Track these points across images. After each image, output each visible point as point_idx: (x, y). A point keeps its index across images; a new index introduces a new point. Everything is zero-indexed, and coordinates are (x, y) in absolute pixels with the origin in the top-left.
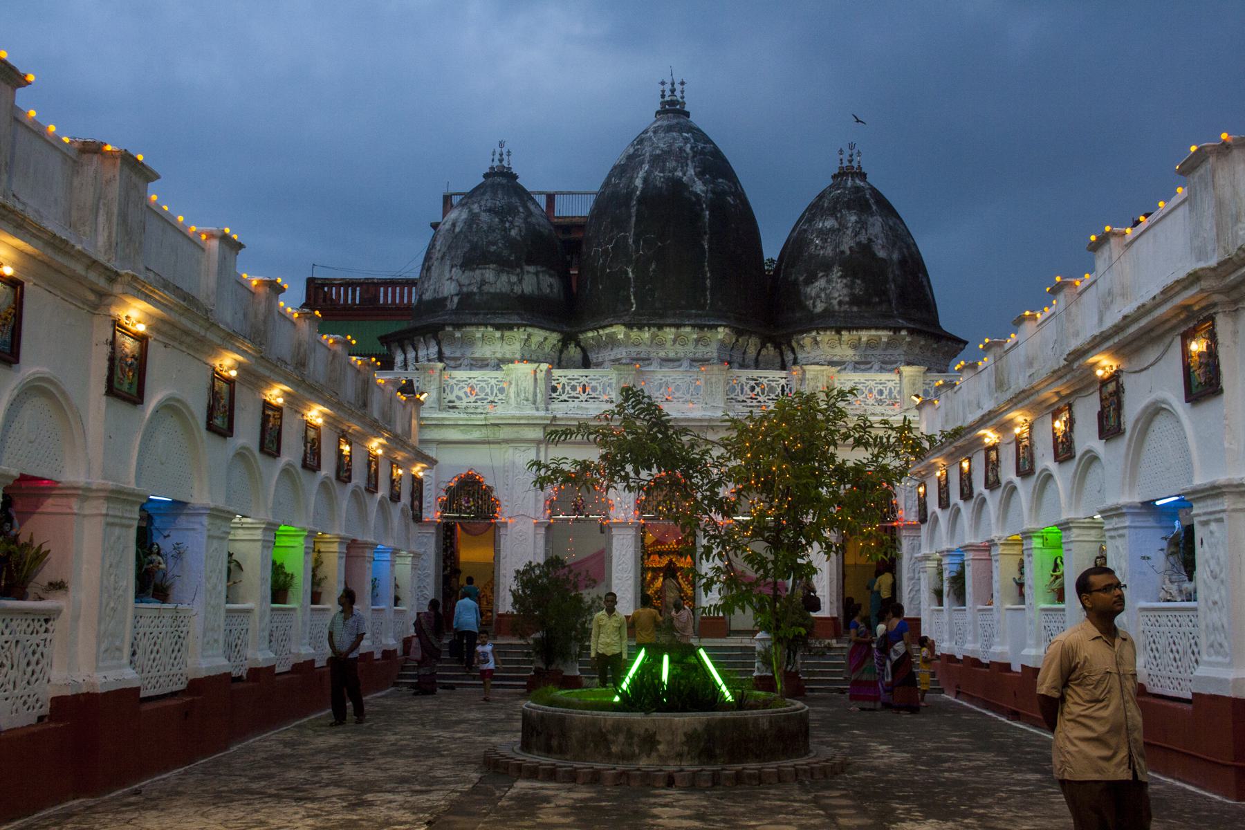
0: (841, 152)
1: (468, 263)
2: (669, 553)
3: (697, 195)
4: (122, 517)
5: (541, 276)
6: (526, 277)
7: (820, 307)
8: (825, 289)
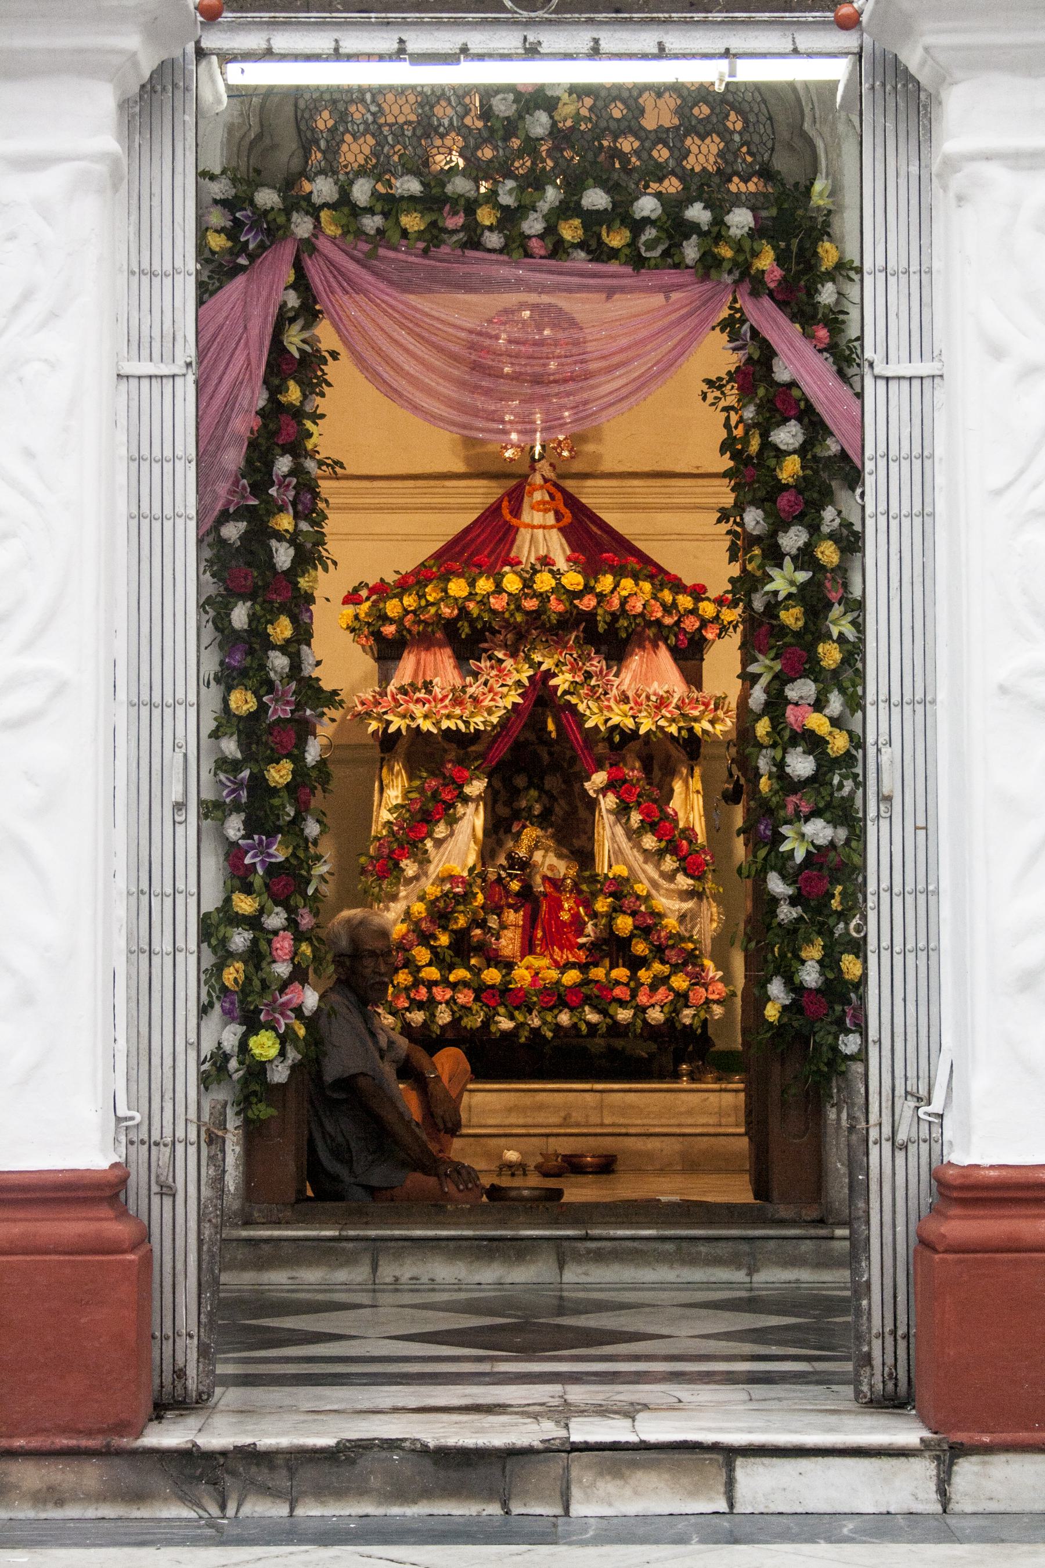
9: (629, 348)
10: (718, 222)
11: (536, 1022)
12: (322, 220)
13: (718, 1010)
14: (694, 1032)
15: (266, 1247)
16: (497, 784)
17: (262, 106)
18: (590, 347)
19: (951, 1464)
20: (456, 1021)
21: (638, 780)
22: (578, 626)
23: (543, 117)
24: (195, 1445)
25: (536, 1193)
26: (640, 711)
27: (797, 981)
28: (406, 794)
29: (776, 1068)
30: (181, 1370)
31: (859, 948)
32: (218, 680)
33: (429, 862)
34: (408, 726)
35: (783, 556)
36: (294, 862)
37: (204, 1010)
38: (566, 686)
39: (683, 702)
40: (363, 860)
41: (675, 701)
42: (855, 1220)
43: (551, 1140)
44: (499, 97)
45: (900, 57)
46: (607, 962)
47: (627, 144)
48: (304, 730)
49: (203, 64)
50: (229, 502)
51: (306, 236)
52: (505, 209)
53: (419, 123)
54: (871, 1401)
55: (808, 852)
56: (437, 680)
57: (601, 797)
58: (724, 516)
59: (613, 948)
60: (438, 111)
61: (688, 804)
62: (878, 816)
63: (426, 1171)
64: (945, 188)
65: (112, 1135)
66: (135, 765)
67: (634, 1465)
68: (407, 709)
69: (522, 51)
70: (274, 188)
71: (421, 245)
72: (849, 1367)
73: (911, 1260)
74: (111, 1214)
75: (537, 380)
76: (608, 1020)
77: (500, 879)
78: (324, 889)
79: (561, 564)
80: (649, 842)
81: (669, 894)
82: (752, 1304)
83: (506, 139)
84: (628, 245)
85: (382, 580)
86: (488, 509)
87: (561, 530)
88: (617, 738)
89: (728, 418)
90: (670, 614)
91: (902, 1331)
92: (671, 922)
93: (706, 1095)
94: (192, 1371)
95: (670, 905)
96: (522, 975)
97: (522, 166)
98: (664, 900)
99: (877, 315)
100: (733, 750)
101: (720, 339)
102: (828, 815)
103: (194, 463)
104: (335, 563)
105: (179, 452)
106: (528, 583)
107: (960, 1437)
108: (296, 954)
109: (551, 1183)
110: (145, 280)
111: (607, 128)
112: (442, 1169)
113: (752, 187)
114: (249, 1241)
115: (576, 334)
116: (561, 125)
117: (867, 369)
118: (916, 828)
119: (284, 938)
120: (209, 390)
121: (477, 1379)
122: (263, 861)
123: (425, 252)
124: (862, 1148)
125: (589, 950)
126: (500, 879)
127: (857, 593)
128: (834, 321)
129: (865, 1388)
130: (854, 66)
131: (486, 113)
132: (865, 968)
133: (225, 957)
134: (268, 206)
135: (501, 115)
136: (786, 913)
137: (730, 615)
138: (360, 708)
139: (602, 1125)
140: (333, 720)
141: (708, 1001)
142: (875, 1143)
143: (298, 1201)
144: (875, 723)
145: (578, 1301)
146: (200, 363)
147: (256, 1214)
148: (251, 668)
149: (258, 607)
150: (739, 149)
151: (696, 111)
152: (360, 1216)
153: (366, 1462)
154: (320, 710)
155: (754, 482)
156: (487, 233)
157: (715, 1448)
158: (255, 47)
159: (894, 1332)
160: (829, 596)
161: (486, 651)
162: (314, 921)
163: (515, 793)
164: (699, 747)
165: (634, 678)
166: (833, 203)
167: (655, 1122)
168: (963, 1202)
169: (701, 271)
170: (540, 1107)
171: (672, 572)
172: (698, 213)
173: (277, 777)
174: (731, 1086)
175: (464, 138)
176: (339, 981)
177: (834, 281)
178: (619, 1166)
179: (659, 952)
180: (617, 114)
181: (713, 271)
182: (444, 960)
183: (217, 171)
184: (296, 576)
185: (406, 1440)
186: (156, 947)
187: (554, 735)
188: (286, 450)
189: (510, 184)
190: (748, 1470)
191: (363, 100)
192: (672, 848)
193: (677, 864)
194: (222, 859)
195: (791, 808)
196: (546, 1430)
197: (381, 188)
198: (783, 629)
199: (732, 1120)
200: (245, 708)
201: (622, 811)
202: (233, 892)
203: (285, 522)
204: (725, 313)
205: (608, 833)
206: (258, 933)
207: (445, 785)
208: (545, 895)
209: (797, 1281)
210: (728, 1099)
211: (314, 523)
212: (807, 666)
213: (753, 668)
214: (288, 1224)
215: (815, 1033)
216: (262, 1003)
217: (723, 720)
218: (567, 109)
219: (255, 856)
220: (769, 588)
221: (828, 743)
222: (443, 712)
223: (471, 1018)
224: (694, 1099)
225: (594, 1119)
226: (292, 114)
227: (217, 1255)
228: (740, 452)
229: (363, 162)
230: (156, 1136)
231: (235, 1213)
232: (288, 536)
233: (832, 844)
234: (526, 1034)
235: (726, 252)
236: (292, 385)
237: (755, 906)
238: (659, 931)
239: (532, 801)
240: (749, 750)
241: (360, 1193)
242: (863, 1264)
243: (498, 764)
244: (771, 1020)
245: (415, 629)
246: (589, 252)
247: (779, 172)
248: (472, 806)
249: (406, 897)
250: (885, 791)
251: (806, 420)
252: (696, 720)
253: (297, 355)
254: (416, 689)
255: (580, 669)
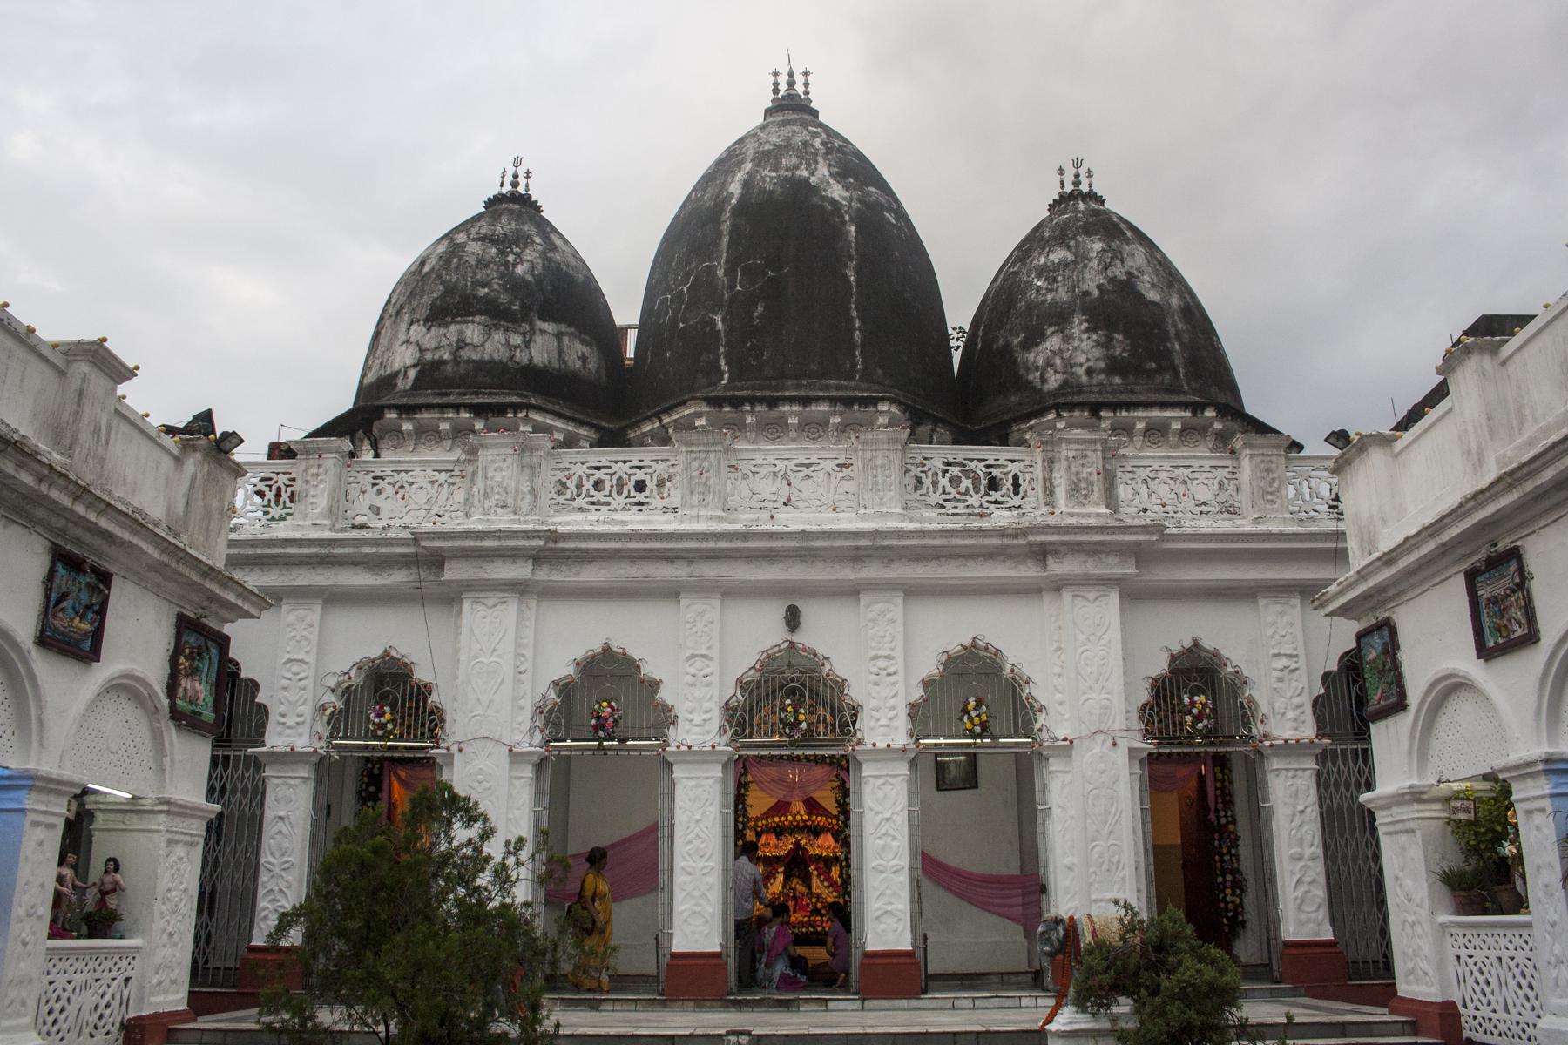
0: (1061, 171)
1: (438, 315)
2: (794, 829)
3: (833, 202)
4: (45, 813)
5: (566, 340)
6: (538, 338)
7: (1054, 381)
8: (1060, 351)
239: (796, 872)
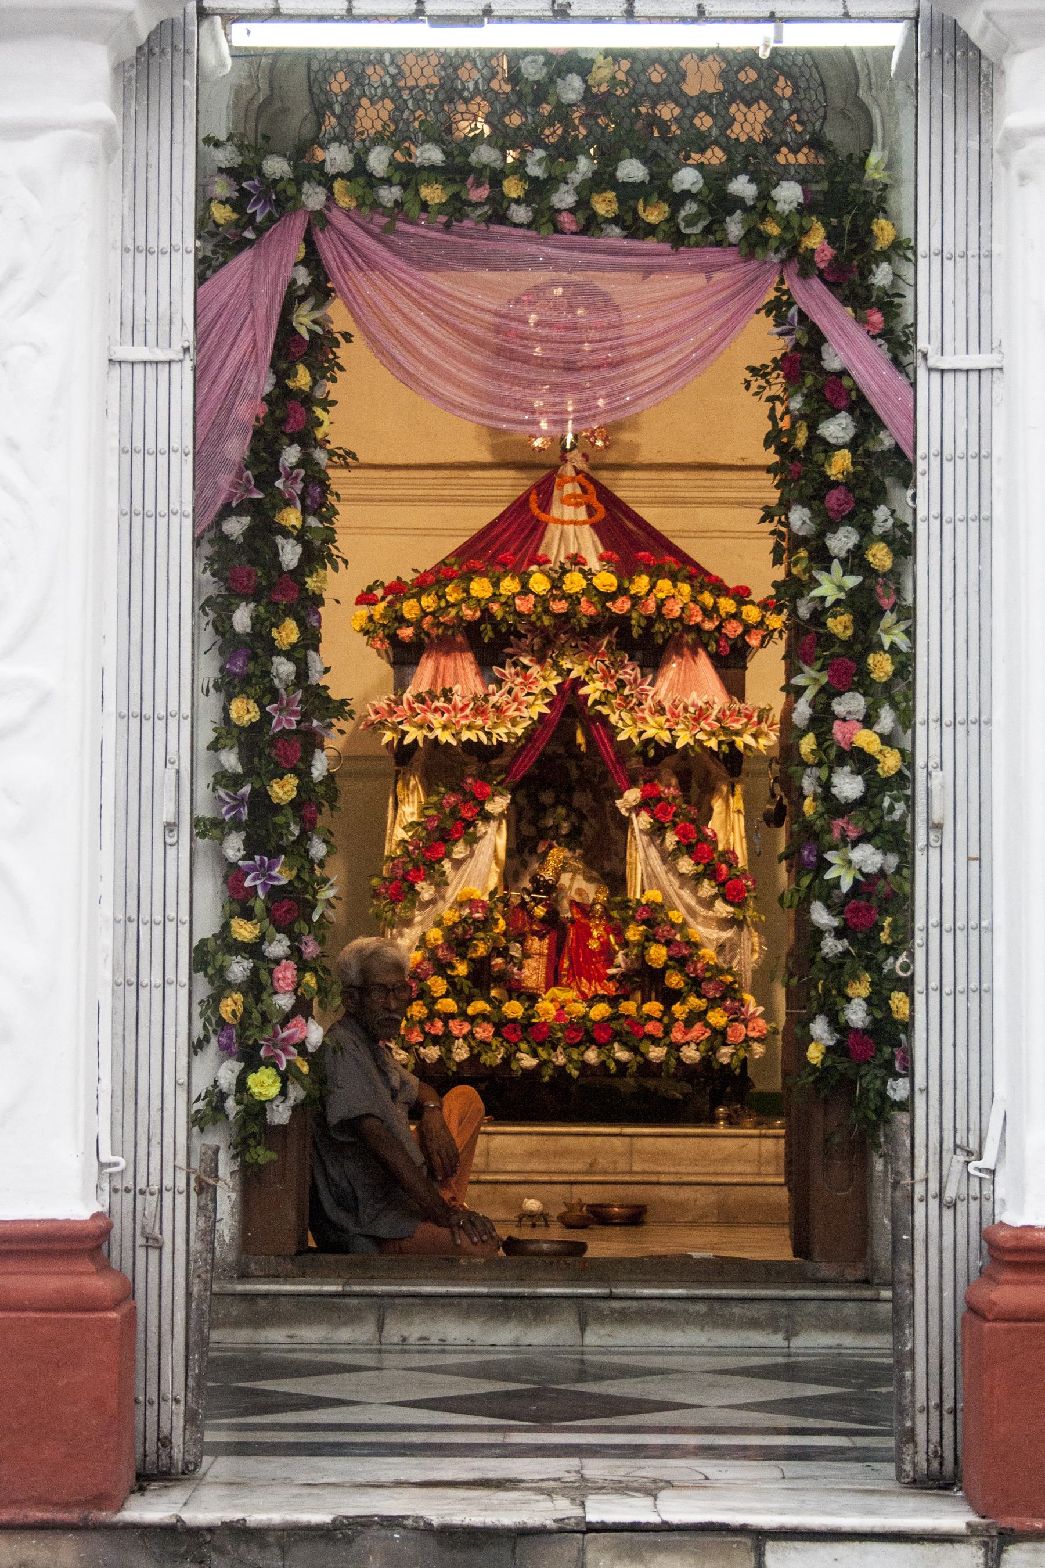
9: (667, 332)
10: (764, 196)
11: (561, 1060)
12: (336, 191)
13: (758, 1049)
14: (732, 1071)
15: (263, 1303)
16: (522, 800)
17: (274, 64)
18: (627, 330)
19: (1001, 1551)
20: (474, 1058)
21: (674, 798)
22: (610, 631)
23: (575, 81)
24: (179, 1520)
25: (556, 1246)
26: (677, 724)
27: (842, 1020)
28: (422, 811)
29: (819, 1116)
30: (166, 1438)
31: (907, 985)
32: (218, 687)
33: (447, 884)
34: (426, 737)
35: (831, 558)
36: (297, 884)
37: (196, 1047)
38: (597, 695)
39: (724, 713)
40: (375, 882)
41: (715, 713)
42: (900, 1282)
43: (575, 1188)
44: (529, 59)
45: (961, 23)
46: (638, 995)
47: (667, 111)
48: (311, 742)
49: (206, 24)
50: (232, 495)
51: (318, 207)
52: (534, 180)
53: (442, 86)
54: (914, 1481)
55: (856, 881)
56: (457, 688)
57: (633, 816)
58: (768, 515)
59: (645, 980)
60: (463, 73)
61: (728, 824)
62: (928, 845)
63: (437, 1221)
64: (1007, 165)
65: (94, 1182)
66: (123, 781)
67: (656, 1548)
68: (424, 719)
69: (550, 14)
70: (285, 156)
71: (442, 219)
72: (890, 1442)
73: (959, 1328)
74: (92, 1268)
75: (571, 367)
76: (640, 1059)
77: (523, 904)
78: (330, 913)
79: (593, 563)
80: (686, 865)
81: (707, 922)
82: (789, 1372)
83: (537, 103)
84: (667, 220)
85: (399, 578)
86: (515, 502)
87: (595, 526)
88: (652, 753)
89: (773, 409)
90: (711, 619)
91: (948, 1404)
92: (709, 953)
93: (744, 1141)
94: (178, 1439)
95: (707, 934)
96: (546, 1008)
97: (553, 133)
98: (700, 928)
99: (933, 300)
100: (776, 767)
101: (766, 323)
102: (877, 840)
103: (191, 456)
104: (346, 562)
105: (175, 445)
106: (556, 584)
107: (1011, 1522)
108: (299, 985)
109: (575, 1236)
110: (140, 258)
111: (646, 94)
112: (454, 1219)
113: (801, 159)
114: (245, 1296)
115: (612, 317)
116: (595, 90)
117: (920, 361)
118: (969, 859)
119: (286, 968)
120: (211, 374)
121: (485, 1451)
122: (264, 884)
123: (447, 227)
124: (907, 1206)
125: (620, 982)
126: (523, 904)
127: (910, 602)
128: (889, 304)
129: (908, 1467)
130: (910, 30)
131: (515, 77)
132: (912, 1010)
133: (222, 986)
134: (277, 176)
135: (531, 78)
136: (831, 946)
137: (775, 621)
138: (373, 717)
139: (631, 1172)
140: (342, 732)
141: (748, 1039)
142: (921, 1200)
143: (299, 1253)
144: (926, 743)
145: (602, 1366)
146: (198, 349)
147: (252, 1266)
148: (253, 674)
149: (261, 609)
150: (788, 117)
151: (742, 76)
152: (364, 1270)
153: (366, 1540)
154: (328, 720)
155: (800, 478)
156: (514, 206)
157: (743, 1530)
158: (262, 7)
159: (940, 1406)
160: (881, 602)
161: (511, 656)
162: (319, 950)
163: (541, 810)
164: (741, 763)
165: (670, 688)
166: (890, 177)
167: (689, 1169)
168: (1016, 1266)
169: (745, 250)
170: (565, 1152)
171: (714, 573)
172: (742, 187)
173: (281, 793)
174: (771, 1132)
175: (490, 104)
176: (348, 1014)
177: (889, 260)
178: (648, 1218)
179: (696, 985)
180: (656, 78)
181: (759, 251)
182: (461, 991)
183: (223, 137)
184: (303, 575)
185: (408, 1517)
186: (144, 979)
187: (583, 748)
188: (293, 440)
189: (540, 153)
190: (780, 1556)
191: (381, 62)
192: (710, 872)
193: (716, 890)
194: (220, 881)
195: (837, 833)
196: (562, 1509)
197: (399, 157)
198: (831, 637)
199: (772, 1169)
200: (247, 718)
201: (657, 831)
202: (231, 917)
203: (292, 517)
204: (772, 295)
205: (641, 854)
206: (259, 963)
207: (465, 802)
208: (573, 921)
209: (839, 1347)
210: (769, 1145)
211: (323, 519)
212: (856, 679)
213: (798, 680)
214: (287, 1277)
215: (861, 1077)
216: (263, 1038)
217: (767, 735)
218: (602, 73)
219: (255, 879)
220: (816, 593)
221: (878, 762)
222: (463, 722)
223: (490, 1054)
224: (730, 1146)
225: (623, 1166)
226: (304, 76)
227: (207, 1311)
228: (787, 445)
229: (380, 129)
230: (141, 1184)
231: (230, 1265)
232: (295, 532)
233: (882, 873)
234: (550, 1072)
235: (773, 229)
236: (301, 369)
237: (797, 939)
238: (695, 962)
239: (559, 818)
240: (793, 769)
241: (362, 1243)
242: (907, 1332)
243: (523, 777)
244: (814, 1062)
245: (434, 632)
246: (623, 228)
247: (830, 143)
248: (493, 824)
249: (421, 923)
250: (936, 818)
251: (857, 412)
252: (738, 733)
253: (307, 337)
254: (434, 697)
255: (612, 678)
